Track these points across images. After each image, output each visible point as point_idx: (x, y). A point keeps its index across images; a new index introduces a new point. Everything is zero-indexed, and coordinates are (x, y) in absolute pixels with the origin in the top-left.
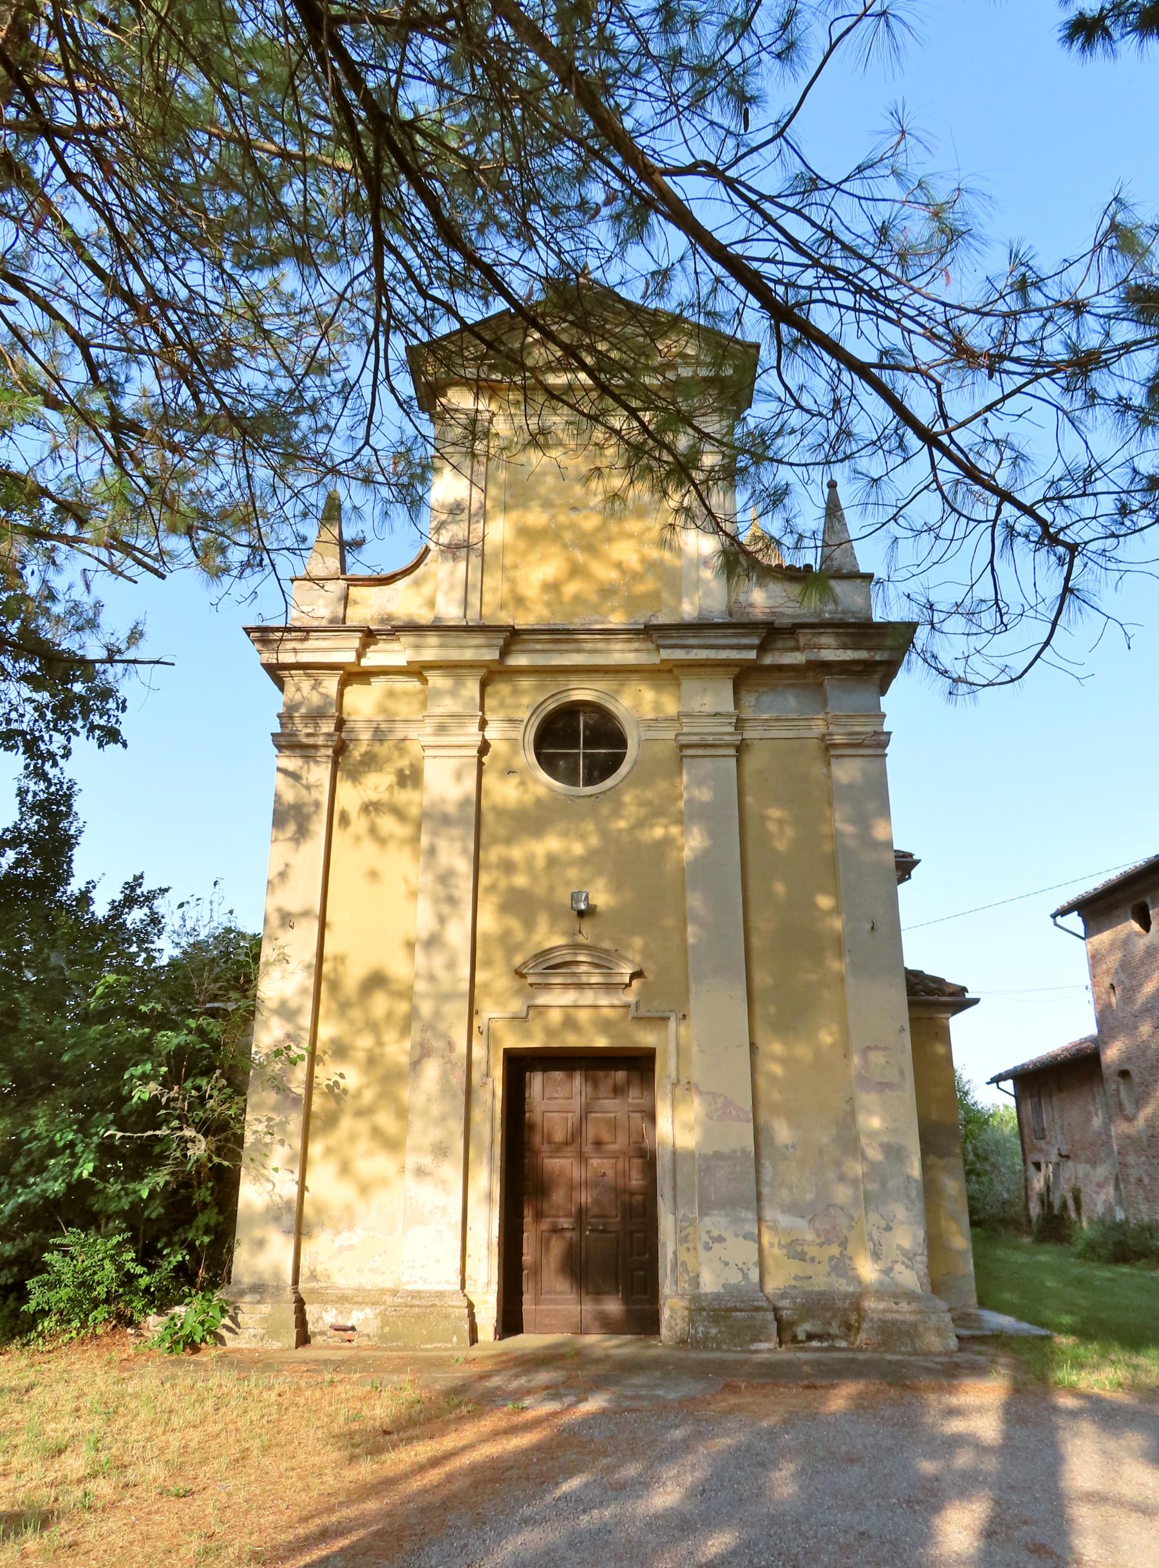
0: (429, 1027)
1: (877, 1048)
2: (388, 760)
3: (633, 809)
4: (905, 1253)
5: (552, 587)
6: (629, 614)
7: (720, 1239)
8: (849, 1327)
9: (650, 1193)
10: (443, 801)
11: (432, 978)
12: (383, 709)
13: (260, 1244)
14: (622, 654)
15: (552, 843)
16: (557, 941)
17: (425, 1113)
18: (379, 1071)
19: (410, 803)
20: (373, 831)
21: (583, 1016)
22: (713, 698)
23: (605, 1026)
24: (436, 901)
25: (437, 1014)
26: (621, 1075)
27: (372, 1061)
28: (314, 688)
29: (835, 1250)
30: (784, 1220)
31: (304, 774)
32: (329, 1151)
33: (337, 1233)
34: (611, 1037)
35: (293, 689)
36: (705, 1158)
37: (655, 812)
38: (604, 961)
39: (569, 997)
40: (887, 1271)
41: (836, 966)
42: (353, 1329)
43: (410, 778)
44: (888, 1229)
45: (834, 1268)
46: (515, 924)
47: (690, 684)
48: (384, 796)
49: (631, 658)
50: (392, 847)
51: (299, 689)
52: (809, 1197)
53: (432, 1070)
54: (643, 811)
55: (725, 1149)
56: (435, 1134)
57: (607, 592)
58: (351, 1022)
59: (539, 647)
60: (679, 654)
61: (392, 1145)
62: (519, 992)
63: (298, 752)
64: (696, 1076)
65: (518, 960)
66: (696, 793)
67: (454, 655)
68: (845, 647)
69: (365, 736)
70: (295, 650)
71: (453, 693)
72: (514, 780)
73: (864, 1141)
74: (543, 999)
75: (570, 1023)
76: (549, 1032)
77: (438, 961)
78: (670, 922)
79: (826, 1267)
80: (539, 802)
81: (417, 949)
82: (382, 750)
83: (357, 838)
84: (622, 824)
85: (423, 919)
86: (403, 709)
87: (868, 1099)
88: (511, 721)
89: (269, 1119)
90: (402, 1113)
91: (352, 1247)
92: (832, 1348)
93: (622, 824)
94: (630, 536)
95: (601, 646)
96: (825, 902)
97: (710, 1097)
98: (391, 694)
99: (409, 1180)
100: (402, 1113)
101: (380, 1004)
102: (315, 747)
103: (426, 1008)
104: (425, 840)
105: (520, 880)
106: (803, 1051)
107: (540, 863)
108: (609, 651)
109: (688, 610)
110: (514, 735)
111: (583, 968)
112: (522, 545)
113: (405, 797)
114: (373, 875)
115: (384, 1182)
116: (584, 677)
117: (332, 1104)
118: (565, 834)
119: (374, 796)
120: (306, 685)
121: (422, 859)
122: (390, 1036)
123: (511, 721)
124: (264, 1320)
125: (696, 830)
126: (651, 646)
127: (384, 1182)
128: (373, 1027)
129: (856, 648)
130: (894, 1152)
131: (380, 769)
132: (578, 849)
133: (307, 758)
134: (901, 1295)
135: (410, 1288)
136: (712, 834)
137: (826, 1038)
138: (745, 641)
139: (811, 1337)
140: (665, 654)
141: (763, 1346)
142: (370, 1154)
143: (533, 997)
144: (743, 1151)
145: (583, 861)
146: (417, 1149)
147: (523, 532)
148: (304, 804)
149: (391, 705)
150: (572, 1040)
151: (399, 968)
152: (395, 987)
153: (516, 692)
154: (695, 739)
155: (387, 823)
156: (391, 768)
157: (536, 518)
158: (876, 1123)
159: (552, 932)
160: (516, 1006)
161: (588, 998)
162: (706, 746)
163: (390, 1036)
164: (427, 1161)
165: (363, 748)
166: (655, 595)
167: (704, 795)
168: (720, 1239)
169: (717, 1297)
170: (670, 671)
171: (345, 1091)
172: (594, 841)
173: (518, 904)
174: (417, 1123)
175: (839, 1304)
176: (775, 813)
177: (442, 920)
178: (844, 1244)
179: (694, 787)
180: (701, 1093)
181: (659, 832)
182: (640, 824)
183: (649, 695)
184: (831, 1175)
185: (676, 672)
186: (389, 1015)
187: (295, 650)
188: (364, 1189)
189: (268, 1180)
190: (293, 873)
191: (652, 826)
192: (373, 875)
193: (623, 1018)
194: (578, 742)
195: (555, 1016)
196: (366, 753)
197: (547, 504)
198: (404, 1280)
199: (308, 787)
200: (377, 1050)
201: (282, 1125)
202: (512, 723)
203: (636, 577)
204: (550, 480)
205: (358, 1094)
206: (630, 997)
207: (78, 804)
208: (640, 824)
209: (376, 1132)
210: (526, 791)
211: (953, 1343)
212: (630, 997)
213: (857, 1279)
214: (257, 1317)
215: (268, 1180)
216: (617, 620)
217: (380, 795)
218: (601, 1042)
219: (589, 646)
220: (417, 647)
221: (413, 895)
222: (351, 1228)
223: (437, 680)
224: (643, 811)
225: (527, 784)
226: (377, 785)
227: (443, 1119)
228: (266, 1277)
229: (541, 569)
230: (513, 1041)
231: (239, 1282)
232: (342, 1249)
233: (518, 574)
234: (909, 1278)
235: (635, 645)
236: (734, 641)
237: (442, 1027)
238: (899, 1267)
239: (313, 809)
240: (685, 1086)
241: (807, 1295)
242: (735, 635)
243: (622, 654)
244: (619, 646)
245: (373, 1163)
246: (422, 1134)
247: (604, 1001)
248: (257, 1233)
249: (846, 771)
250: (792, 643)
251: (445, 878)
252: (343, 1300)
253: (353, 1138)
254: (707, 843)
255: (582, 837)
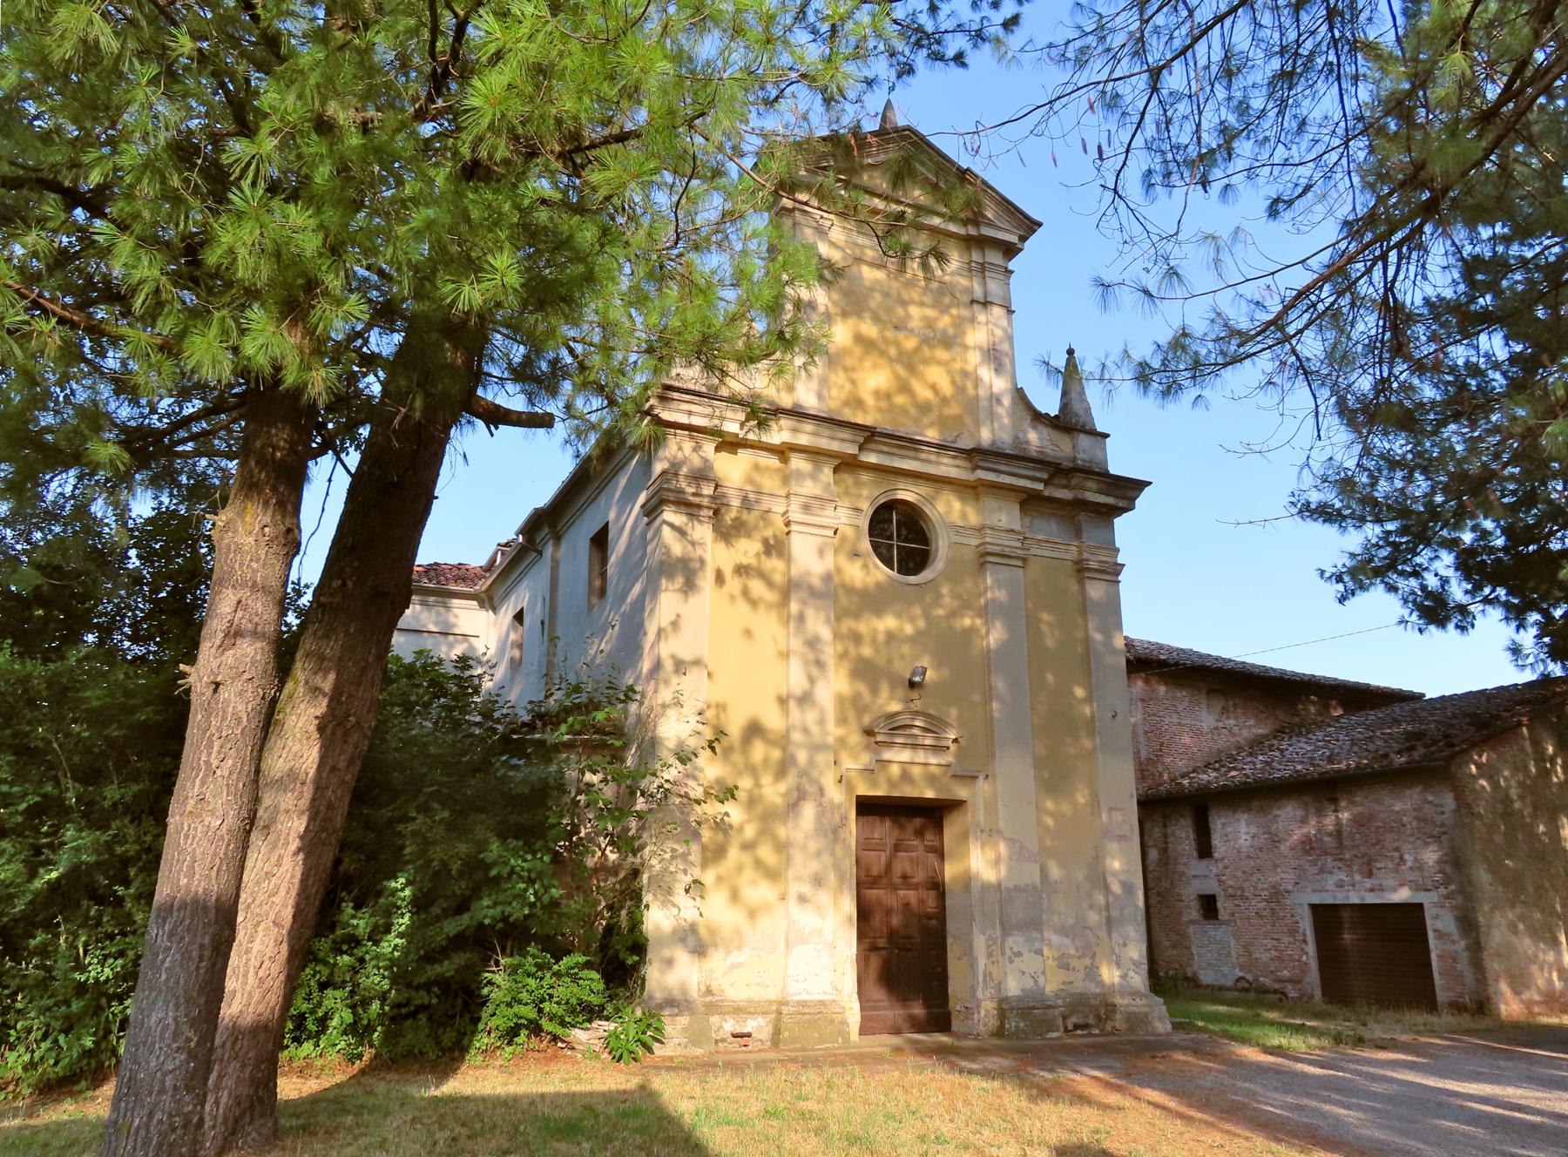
0: (803, 774)
1: (1117, 809)
2: (756, 527)
3: (947, 600)
4: (1134, 963)
5: (883, 396)
6: (941, 432)
7: (1019, 954)
8: (1099, 1018)
9: (941, 915)
10: (809, 573)
11: (806, 730)
12: (750, 481)
13: (670, 962)
14: (948, 467)
15: (888, 622)
16: (895, 707)
17: (804, 848)
18: (759, 809)
19: (774, 570)
20: (745, 592)
21: (916, 771)
22: (1006, 516)
23: (932, 780)
24: (806, 663)
25: (811, 762)
26: (918, 822)
27: (752, 802)
28: (695, 450)
29: (1087, 962)
30: (1055, 939)
31: (689, 531)
32: (719, 879)
33: (729, 952)
34: (936, 790)
35: (675, 447)
36: (1008, 890)
37: (965, 606)
38: (935, 725)
39: (905, 755)
40: (1124, 977)
41: (1087, 743)
42: (749, 1035)
43: (776, 547)
44: (1125, 945)
45: (1087, 975)
46: (863, 689)
47: (990, 502)
48: (753, 562)
49: (953, 472)
50: (762, 608)
51: (680, 448)
52: (1071, 921)
53: (808, 811)
54: (956, 603)
55: (1021, 884)
56: (814, 866)
57: (925, 408)
58: (734, 765)
59: (885, 449)
60: (991, 477)
61: (772, 875)
62: (867, 747)
63: (683, 509)
64: (1002, 825)
65: (867, 720)
66: (997, 593)
67: (824, 443)
68: (1101, 492)
69: (735, 503)
70: (690, 413)
71: (813, 477)
72: (858, 563)
73: (1110, 879)
74: (887, 755)
75: (906, 777)
76: (892, 783)
77: (811, 717)
78: (976, 698)
79: (1081, 975)
80: (878, 585)
81: (792, 704)
82: (750, 518)
83: (733, 598)
84: (941, 612)
85: (795, 677)
86: (770, 483)
87: (1114, 846)
88: (856, 509)
89: (673, 850)
90: (782, 847)
91: (740, 965)
92: (1090, 1035)
93: (941, 612)
94: (939, 363)
95: (933, 457)
96: (1080, 692)
97: (1011, 841)
98: (757, 467)
99: (792, 903)
100: (782, 847)
101: (759, 751)
102: (699, 506)
103: (802, 756)
104: (794, 607)
105: (867, 651)
106: (1066, 808)
107: (881, 638)
108: (938, 463)
109: (986, 436)
110: (857, 522)
111: (916, 731)
112: (858, 351)
113: (774, 565)
114: (748, 633)
115: (767, 907)
116: (910, 480)
117: (720, 837)
118: (898, 615)
119: (745, 561)
120: (688, 446)
121: (792, 625)
122: (766, 780)
123: (856, 509)
124: (685, 1030)
125: (998, 624)
126: (968, 465)
127: (767, 907)
128: (753, 771)
129: (1107, 495)
130: (1128, 888)
131: (749, 536)
132: (909, 629)
133: (692, 516)
134: (1135, 994)
135: (797, 998)
136: (1011, 629)
137: (1081, 798)
138: (1038, 475)
139: (1077, 1027)
140: (981, 474)
141: (1055, 1035)
142: (754, 883)
143: (878, 753)
144: (1034, 886)
145: (913, 640)
146: (799, 879)
147: (859, 338)
148: (691, 560)
149: (757, 478)
150: (909, 792)
151: (773, 720)
152: (772, 737)
153: (858, 484)
154: (996, 549)
155: (757, 587)
156: (757, 536)
157: (870, 329)
158: (1116, 865)
159: (892, 698)
160: (865, 759)
161: (921, 756)
162: (1009, 557)
163: (766, 780)
164: (807, 889)
165: (733, 514)
166: (958, 419)
167: (1001, 595)
168: (1019, 954)
169: (1019, 999)
170: (974, 488)
171: (731, 827)
172: (922, 624)
173: (864, 671)
174: (798, 857)
175: (1093, 1002)
176: (1045, 617)
177: (812, 680)
178: (1093, 957)
179: (993, 586)
180: (1006, 839)
181: (967, 622)
182: (953, 614)
183: (957, 505)
184: (1085, 905)
185: (980, 489)
186: (766, 760)
187: (690, 413)
188: (752, 914)
189: (674, 905)
190: (683, 623)
191: (962, 616)
192: (748, 633)
193: (945, 774)
194: (901, 536)
195: (895, 770)
196: (736, 519)
197: (877, 319)
198: (791, 991)
199: (693, 544)
200: (756, 791)
201: (685, 856)
202: (848, 515)
203: (945, 401)
204: (878, 296)
205: (741, 829)
206: (948, 758)
207: (722, 545)
208: (953, 614)
209: (759, 864)
210: (868, 573)
211: (1169, 1027)
212: (948, 758)
213: (1101, 983)
214: (679, 1027)
215: (674, 905)
216: (932, 435)
217: (749, 560)
218: (930, 794)
219: (924, 456)
220: (794, 430)
221: (785, 655)
222: (740, 948)
223: (798, 463)
224: (956, 603)
225: (870, 572)
226: (747, 549)
227: (818, 854)
228: (676, 992)
229: (875, 378)
230: (863, 790)
231: (651, 998)
232: (733, 966)
233: (856, 376)
234: (1139, 980)
235: (958, 462)
236: (1030, 473)
237: (815, 774)
238: (1131, 974)
239: (698, 565)
240: (990, 833)
241: (1072, 995)
242: (1034, 469)
243: (948, 467)
244: (946, 460)
245: (759, 891)
246: (803, 866)
247: (933, 760)
248: (667, 953)
249: (1095, 591)
250: (1064, 482)
251: (813, 643)
252: (739, 1011)
253: (739, 869)
254: (1005, 637)
255: (912, 620)
